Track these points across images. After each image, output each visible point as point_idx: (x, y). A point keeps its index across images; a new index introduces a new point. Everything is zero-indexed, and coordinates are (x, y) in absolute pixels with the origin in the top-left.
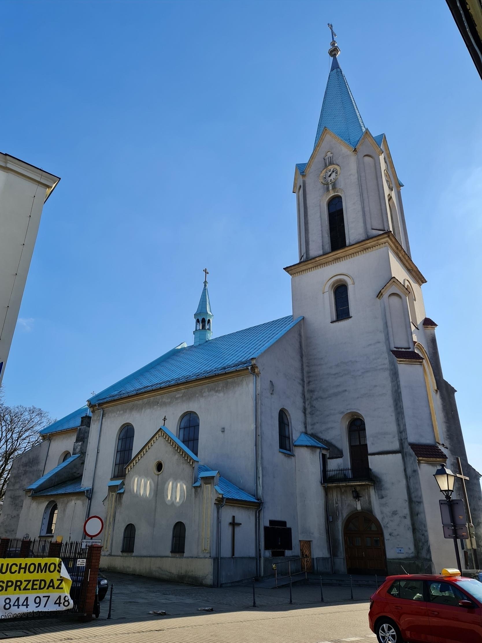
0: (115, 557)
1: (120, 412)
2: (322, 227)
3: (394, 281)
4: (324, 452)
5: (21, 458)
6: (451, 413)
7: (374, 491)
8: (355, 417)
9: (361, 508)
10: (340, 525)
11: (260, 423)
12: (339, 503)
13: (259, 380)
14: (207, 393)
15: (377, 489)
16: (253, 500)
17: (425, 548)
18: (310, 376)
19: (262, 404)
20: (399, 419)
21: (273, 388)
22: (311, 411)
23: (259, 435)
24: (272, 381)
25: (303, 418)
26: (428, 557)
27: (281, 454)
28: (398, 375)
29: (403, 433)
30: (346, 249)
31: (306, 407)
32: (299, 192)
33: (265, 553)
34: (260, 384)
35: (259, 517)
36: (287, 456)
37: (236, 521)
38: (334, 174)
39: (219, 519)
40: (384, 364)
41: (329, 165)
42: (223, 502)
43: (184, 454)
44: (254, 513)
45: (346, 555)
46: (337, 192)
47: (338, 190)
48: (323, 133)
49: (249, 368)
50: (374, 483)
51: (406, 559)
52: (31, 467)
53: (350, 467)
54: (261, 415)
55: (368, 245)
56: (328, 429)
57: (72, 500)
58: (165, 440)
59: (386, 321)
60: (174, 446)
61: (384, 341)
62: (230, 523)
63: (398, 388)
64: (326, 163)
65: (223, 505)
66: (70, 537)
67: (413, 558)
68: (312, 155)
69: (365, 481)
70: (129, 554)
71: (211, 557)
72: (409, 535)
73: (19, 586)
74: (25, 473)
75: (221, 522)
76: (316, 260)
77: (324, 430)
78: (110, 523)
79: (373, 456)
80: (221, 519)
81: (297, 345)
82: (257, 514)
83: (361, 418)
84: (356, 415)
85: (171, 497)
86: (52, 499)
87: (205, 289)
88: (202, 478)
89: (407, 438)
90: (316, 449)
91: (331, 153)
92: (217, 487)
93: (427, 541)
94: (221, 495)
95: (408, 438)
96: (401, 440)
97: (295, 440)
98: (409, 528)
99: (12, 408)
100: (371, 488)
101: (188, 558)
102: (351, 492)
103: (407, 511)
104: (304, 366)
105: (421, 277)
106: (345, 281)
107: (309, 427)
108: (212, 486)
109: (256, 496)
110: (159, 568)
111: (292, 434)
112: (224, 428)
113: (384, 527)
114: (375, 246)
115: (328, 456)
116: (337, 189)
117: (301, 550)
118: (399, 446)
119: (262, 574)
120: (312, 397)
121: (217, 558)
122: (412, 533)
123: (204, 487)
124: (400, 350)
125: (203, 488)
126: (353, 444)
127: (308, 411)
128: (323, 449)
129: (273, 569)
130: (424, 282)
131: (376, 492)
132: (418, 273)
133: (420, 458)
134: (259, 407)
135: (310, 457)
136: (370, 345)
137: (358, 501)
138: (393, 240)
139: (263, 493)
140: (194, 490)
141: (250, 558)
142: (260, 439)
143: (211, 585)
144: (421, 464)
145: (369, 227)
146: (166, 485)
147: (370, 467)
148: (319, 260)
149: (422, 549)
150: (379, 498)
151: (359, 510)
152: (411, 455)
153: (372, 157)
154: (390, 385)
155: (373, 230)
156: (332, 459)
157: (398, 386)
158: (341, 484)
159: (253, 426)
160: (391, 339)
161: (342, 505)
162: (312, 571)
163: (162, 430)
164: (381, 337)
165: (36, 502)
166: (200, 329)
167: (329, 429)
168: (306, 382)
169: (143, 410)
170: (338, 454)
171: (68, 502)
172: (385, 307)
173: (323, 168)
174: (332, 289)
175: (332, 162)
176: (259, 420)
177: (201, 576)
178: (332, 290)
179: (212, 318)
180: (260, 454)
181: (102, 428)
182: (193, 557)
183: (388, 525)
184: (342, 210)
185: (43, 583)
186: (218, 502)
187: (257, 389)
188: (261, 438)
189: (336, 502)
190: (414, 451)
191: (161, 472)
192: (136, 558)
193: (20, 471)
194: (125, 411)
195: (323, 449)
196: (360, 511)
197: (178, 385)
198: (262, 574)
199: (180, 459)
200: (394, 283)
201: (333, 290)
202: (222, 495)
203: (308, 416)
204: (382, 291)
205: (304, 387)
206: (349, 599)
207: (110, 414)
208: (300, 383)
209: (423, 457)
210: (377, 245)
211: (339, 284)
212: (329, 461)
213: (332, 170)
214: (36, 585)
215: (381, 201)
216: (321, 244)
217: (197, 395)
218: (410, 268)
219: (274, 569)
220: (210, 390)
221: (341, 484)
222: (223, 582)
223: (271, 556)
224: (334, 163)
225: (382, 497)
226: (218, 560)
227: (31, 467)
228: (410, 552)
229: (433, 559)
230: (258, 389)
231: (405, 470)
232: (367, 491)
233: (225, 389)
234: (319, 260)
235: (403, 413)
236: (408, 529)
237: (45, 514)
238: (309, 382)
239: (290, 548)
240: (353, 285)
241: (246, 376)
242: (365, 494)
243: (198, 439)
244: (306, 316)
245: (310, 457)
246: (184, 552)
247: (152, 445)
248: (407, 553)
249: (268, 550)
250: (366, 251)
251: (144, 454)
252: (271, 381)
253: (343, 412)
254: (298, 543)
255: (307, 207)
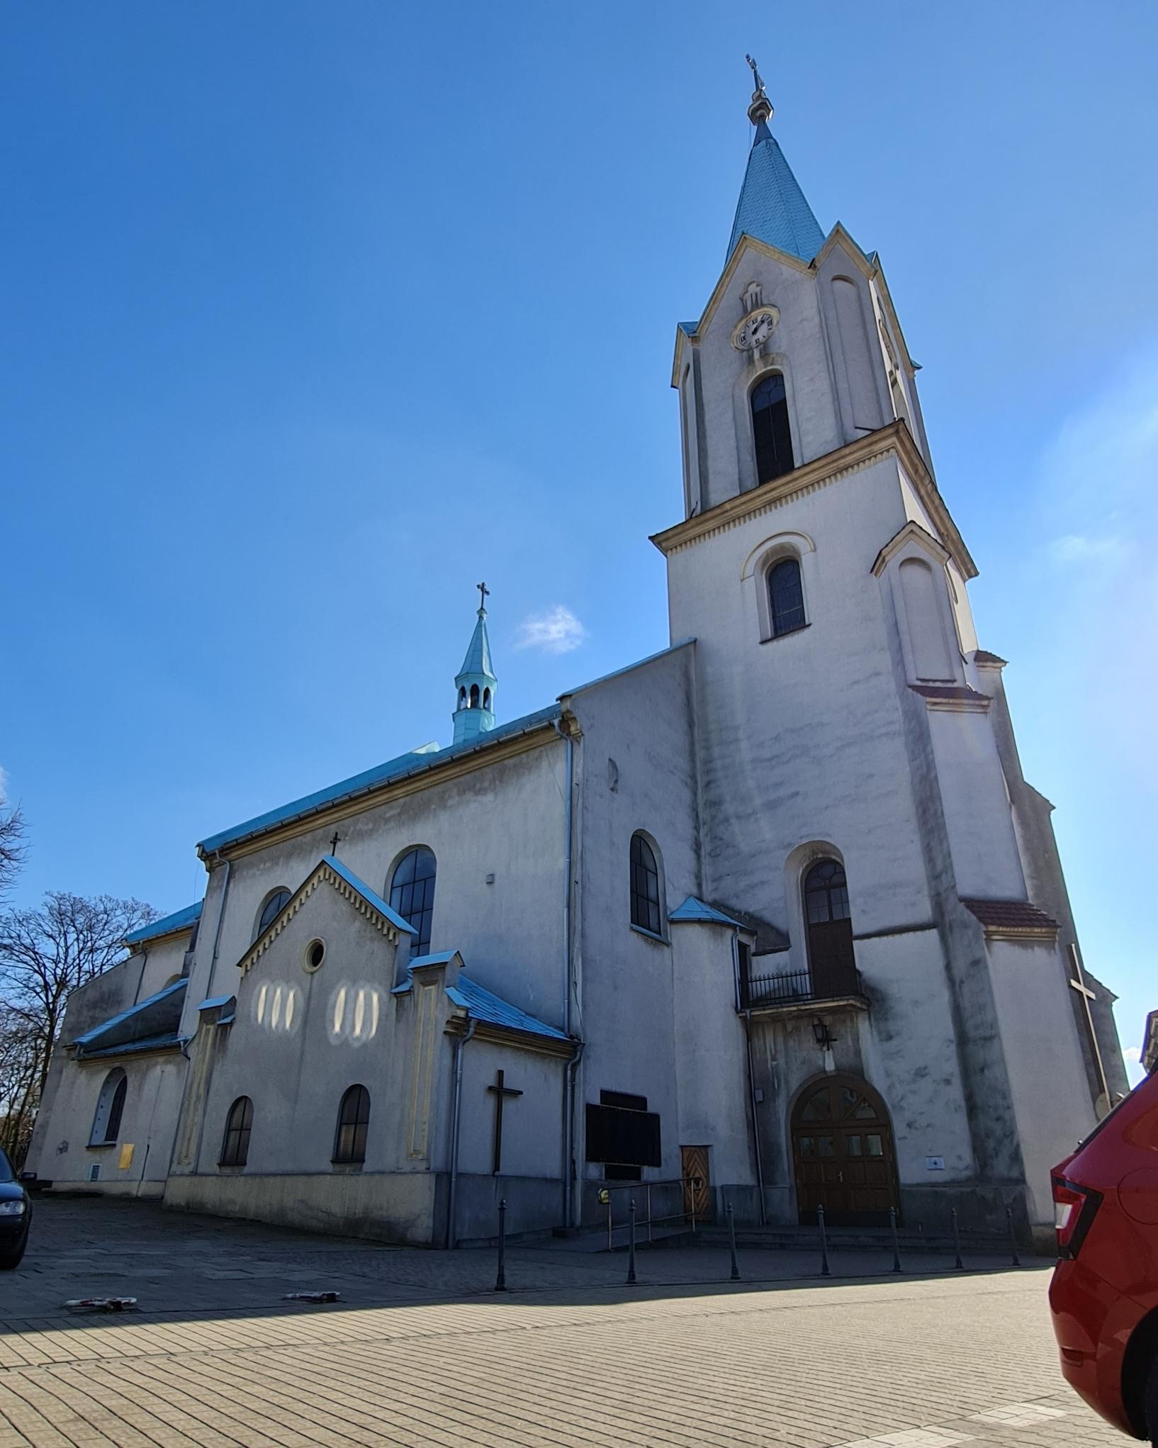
0: (204, 1178)
1: (265, 864)
3: (912, 531)
4: (744, 939)
5: (85, 991)
7: (867, 1023)
8: (820, 856)
10: (781, 1109)
11: (579, 852)
13: (579, 751)
15: (875, 1019)
16: (559, 1035)
21: (617, 775)
25: (694, 862)
26: (1015, 1174)
27: (634, 935)
28: (929, 736)
29: (944, 876)
30: (796, 474)
31: (702, 839)
32: (684, 381)
33: (586, 1168)
34: (582, 761)
35: (573, 1079)
36: (652, 943)
37: (507, 1085)
38: (765, 326)
39: (456, 1073)
40: (891, 723)
42: (468, 1031)
43: (374, 917)
44: (560, 1069)
45: (796, 1180)
46: (772, 364)
47: (773, 358)
49: (556, 722)
53: (806, 968)
54: (583, 833)
55: (848, 459)
56: (752, 887)
57: (156, 1065)
59: (896, 620)
61: (891, 670)
62: (490, 1088)
63: (929, 771)
66: (148, 1146)
67: (968, 1179)
68: (714, 294)
69: (848, 997)
70: (236, 1169)
71: (429, 1169)
72: (960, 1122)
74: (92, 1022)
75: (461, 1081)
76: (725, 509)
78: (198, 1097)
80: (461, 1075)
81: (680, 697)
82: (569, 1072)
83: (834, 857)
86: (117, 1064)
87: (479, 625)
88: (416, 970)
89: (954, 887)
90: (724, 929)
91: (757, 286)
92: (452, 992)
93: (1010, 1133)
94: (462, 1009)
95: (957, 886)
96: (938, 894)
98: (960, 1107)
99: (86, 899)
101: (372, 1173)
102: (811, 1028)
103: (951, 1066)
104: (697, 747)
106: (793, 548)
107: (707, 888)
108: (441, 987)
110: (302, 1201)
111: (665, 894)
112: (492, 875)
113: (894, 1107)
114: (864, 461)
115: (753, 948)
116: (772, 356)
117: (683, 1168)
118: (930, 913)
120: (714, 818)
121: (446, 1173)
122: (965, 1119)
125: (418, 995)
126: (814, 921)
129: (600, 1202)
130: (973, 574)
131: (873, 1025)
132: (960, 547)
136: (856, 682)
137: (828, 1050)
141: (547, 1180)
142: (580, 891)
143: (427, 1243)
144: (995, 943)
145: (848, 424)
146: (332, 998)
147: (858, 966)
148: (731, 509)
149: (996, 1157)
150: (881, 1040)
151: (831, 1072)
152: (965, 926)
153: (851, 283)
155: (858, 430)
157: (930, 765)
158: (785, 1009)
159: (562, 862)
160: (909, 659)
161: (787, 1063)
162: (710, 1217)
163: (326, 866)
164: (884, 661)
166: (467, 708)
167: (756, 885)
169: (314, 853)
170: (780, 942)
171: (148, 1069)
173: (739, 317)
174: (762, 569)
175: (759, 302)
176: (578, 846)
177: (402, 1220)
178: (762, 574)
181: (228, 904)
182: (383, 1173)
183: (904, 1104)
184: (785, 399)
186: (455, 1028)
187: (574, 773)
188: (583, 888)
189: (771, 1055)
190: (974, 913)
191: (319, 966)
193: (82, 1019)
195: (740, 932)
196: (833, 1074)
198: (578, 1221)
202: (467, 1010)
203: (706, 861)
204: (883, 552)
205: (695, 794)
206: (950, 1268)
208: (686, 783)
210: (870, 459)
211: (779, 557)
213: (759, 319)
216: (737, 476)
217: (433, 807)
218: (942, 530)
219: (604, 1201)
220: (462, 792)
221: (785, 1009)
222: (465, 1237)
223: (604, 1178)
224: (765, 302)
225: (890, 1038)
226: (451, 1178)
228: (962, 1165)
231: (948, 967)
232: (849, 1024)
233: (497, 783)
234: (731, 509)
235: (942, 827)
236: (956, 1110)
237: (103, 1098)
239: (656, 1162)
240: (813, 554)
242: (846, 1031)
243: (432, 909)
244: (702, 636)
246: (363, 1161)
247: (301, 904)
248: (953, 1168)
249: (595, 1163)
251: (283, 927)
252: (610, 760)
253: (789, 845)
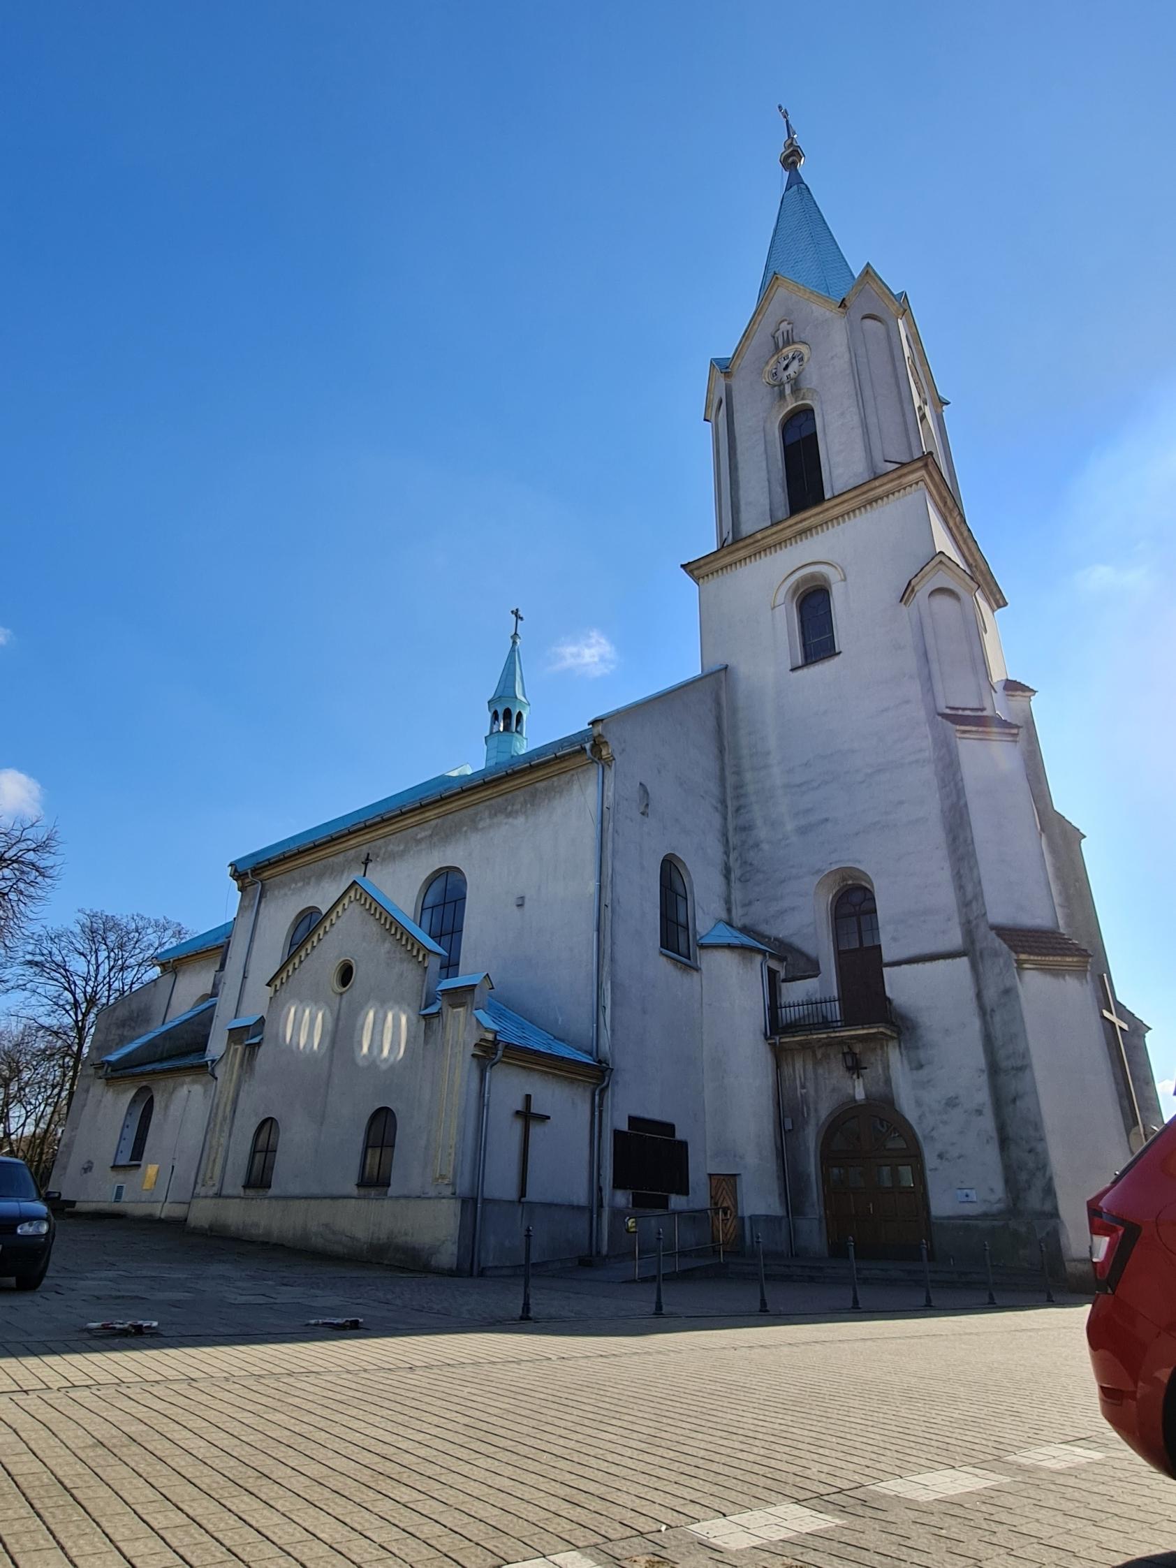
1: (296, 884)
2: (768, 472)
3: (941, 562)
4: (774, 965)
6: (1075, 886)
7: (897, 1051)
8: (850, 882)
9: (866, 1095)
10: (811, 1139)
12: (810, 1086)
13: (610, 774)
14: (488, 820)
17: (1039, 1183)
18: (742, 795)
19: (616, 831)
20: (962, 871)
21: (648, 798)
22: (742, 875)
23: (606, 905)
24: (645, 784)
26: (1048, 1207)
27: (664, 959)
28: (959, 764)
29: (974, 904)
30: (826, 505)
31: (731, 865)
32: (717, 415)
33: (613, 1196)
35: (601, 1105)
36: (681, 968)
38: (796, 362)
39: (484, 1096)
41: (784, 347)
42: (496, 1054)
44: (588, 1095)
46: (803, 399)
47: (804, 395)
48: (771, 285)
49: (588, 746)
50: (899, 1033)
51: (985, 1216)
52: (134, 1029)
53: (835, 993)
56: (783, 912)
58: (362, 908)
60: (383, 922)
63: (959, 798)
64: (777, 345)
65: (496, 1060)
66: (173, 1167)
68: (746, 331)
70: (261, 1192)
72: (992, 1155)
75: (488, 1105)
76: (756, 539)
77: (773, 916)
78: (224, 1118)
79: (896, 969)
80: (489, 1098)
82: (597, 1098)
83: (864, 884)
84: (851, 878)
85: (370, 1048)
86: (144, 1084)
87: (513, 650)
88: (446, 992)
89: (985, 914)
90: (753, 954)
91: (789, 324)
92: (480, 1014)
93: (1043, 1166)
95: (988, 914)
96: (969, 922)
97: (703, 934)
98: (992, 1138)
100: (891, 1044)
103: (983, 1097)
104: (727, 773)
105: (995, 590)
107: (737, 913)
109: (595, 1054)
110: (326, 1225)
112: (522, 898)
114: (893, 494)
115: (782, 975)
116: (802, 391)
119: (605, 1249)
120: (744, 843)
121: (472, 1198)
123: (450, 1013)
124: (960, 712)
125: (447, 1016)
127: (736, 873)
129: (628, 1231)
131: (904, 1052)
133: (1023, 957)
134: (610, 839)
135: (739, 973)
136: (886, 710)
137: (858, 1078)
139: (612, 1047)
140: (423, 1023)
145: (878, 457)
147: (888, 993)
148: (763, 538)
151: (861, 1100)
152: (996, 954)
153: (880, 321)
154: (937, 796)
155: (888, 464)
156: (794, 981)
159: (592, 886)
161: (816, 1091)
163: (357, 886)
165: (114, 1091)
166: (499, 731)
167: (786, 911)
168: (730, 809)
170: (811, 968)
171: (174, 1089)
172: (920, 619)
176: (608, 870)
178: (792, 602)
179: (528, 708)
180: (608, 951)
183: (934, 1134)
187: (605, 797)
188: (613, 912)
191: (348, 987)
192: (274, 1202)
194: (306, 880)
196: (863, 1102)
197: (423, 807)
198: (605, 1249)
199: (395, 952)
200: (940, 566)
201: (795, 600)
202: (496, 1033)
203: (736, 885)
205: (725, 819)
207: (276, 893)
209: (1030, 954)
210: (899, 491)
212: (785, 987)
213: (790, 356)
215: (905, 406)
216: (768, 508)
217: (465, 829)
218: (971, 561)
221: (815, 1037)
222: (490, 1265)
223: (630, 1206)
224: (796, 339)
226: (477, 1204)
227: (134, 1029)
228: (994, 1198)
229: (1062, 1212)
230: (608, 796)
231: (979, 995)
232: (879, 1052)
234: (763, 538)
236: (988, 1141)
237: (128, 1117)
238: (738, 810)
240: (843, 583)
241: (580, 770)
244: (732, 662)
245: (739, 973)
250: (871, 507)
252: (641, 784)
253: (819, 871)
254: (706, 1180)
255: (735, 437)
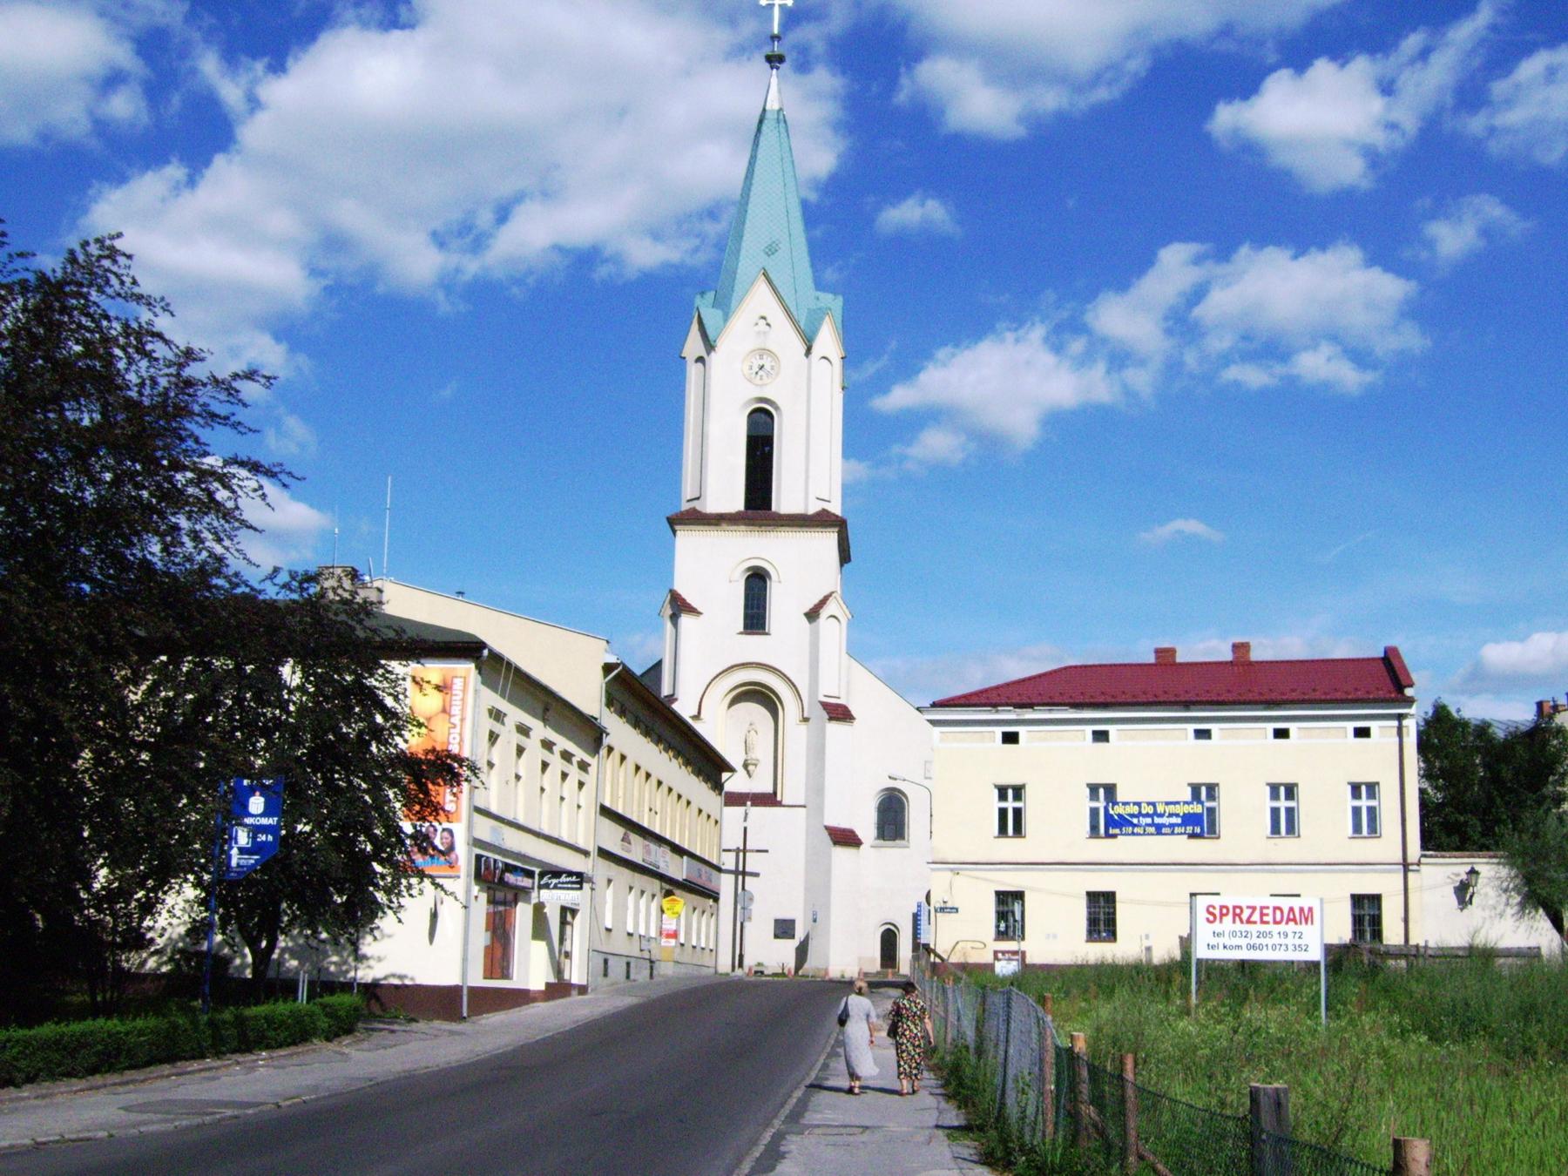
73: (1239, 915)
128: (753, 804)
138: (520, 883)
139: (56, 1135)
152: (218, 490)
185: (1278, 913)
214: (1267, 915)
